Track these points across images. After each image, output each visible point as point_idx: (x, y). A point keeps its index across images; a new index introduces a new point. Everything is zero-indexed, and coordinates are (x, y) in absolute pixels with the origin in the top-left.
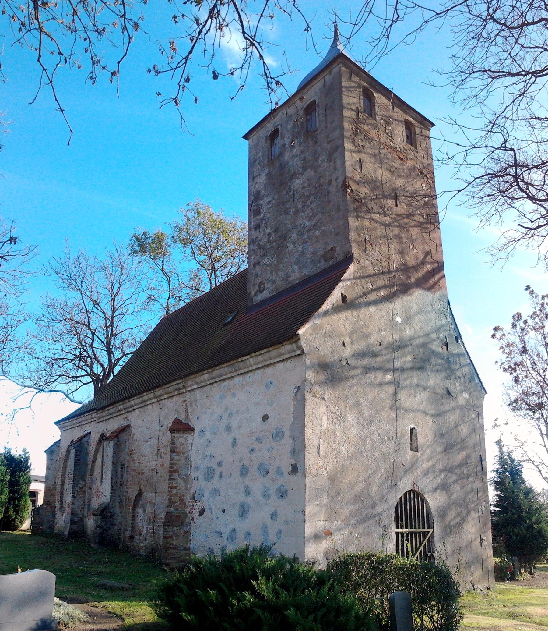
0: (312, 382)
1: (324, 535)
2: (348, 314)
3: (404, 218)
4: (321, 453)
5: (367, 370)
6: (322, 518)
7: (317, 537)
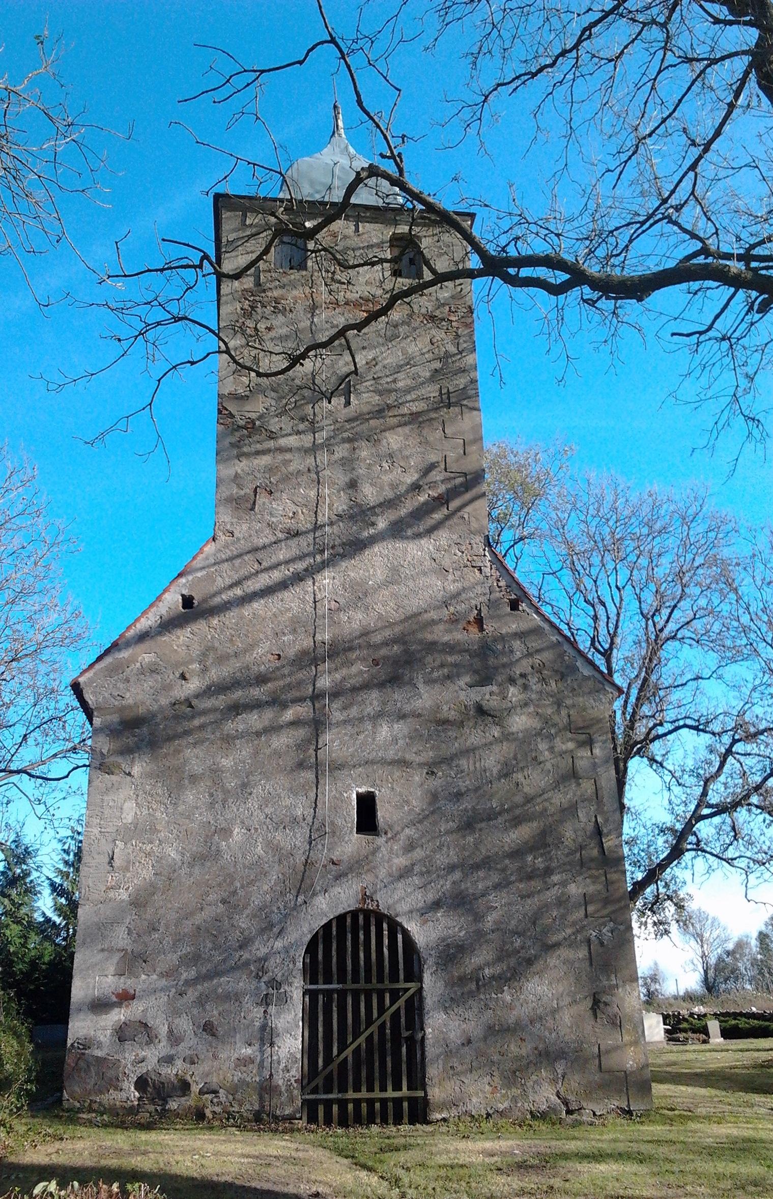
0: (105, 751)
1: (115, 999)
2: (201, 626)
3: (368, 420)
4: (117, 863)
5: (236, 709)
6: (112, 969)
7: (100, 1006)
